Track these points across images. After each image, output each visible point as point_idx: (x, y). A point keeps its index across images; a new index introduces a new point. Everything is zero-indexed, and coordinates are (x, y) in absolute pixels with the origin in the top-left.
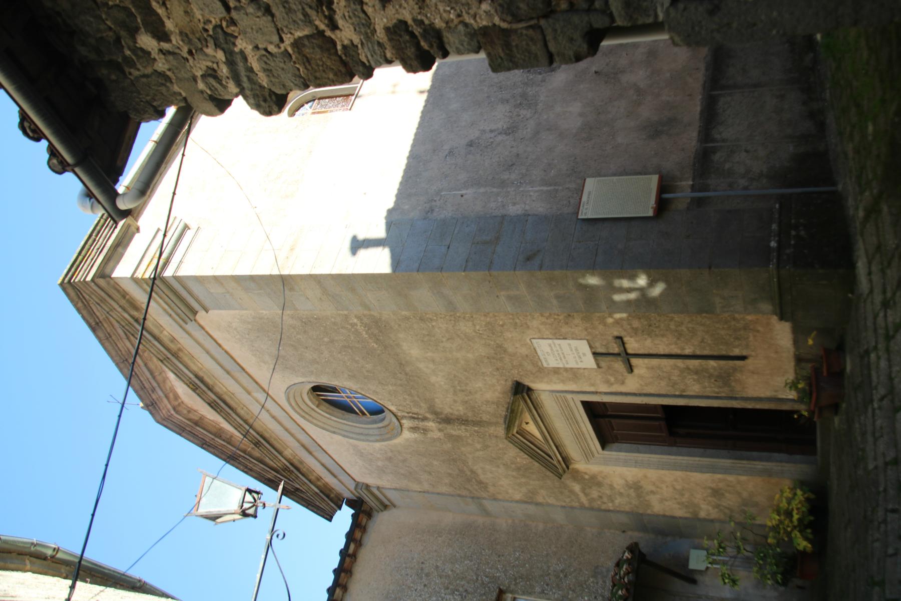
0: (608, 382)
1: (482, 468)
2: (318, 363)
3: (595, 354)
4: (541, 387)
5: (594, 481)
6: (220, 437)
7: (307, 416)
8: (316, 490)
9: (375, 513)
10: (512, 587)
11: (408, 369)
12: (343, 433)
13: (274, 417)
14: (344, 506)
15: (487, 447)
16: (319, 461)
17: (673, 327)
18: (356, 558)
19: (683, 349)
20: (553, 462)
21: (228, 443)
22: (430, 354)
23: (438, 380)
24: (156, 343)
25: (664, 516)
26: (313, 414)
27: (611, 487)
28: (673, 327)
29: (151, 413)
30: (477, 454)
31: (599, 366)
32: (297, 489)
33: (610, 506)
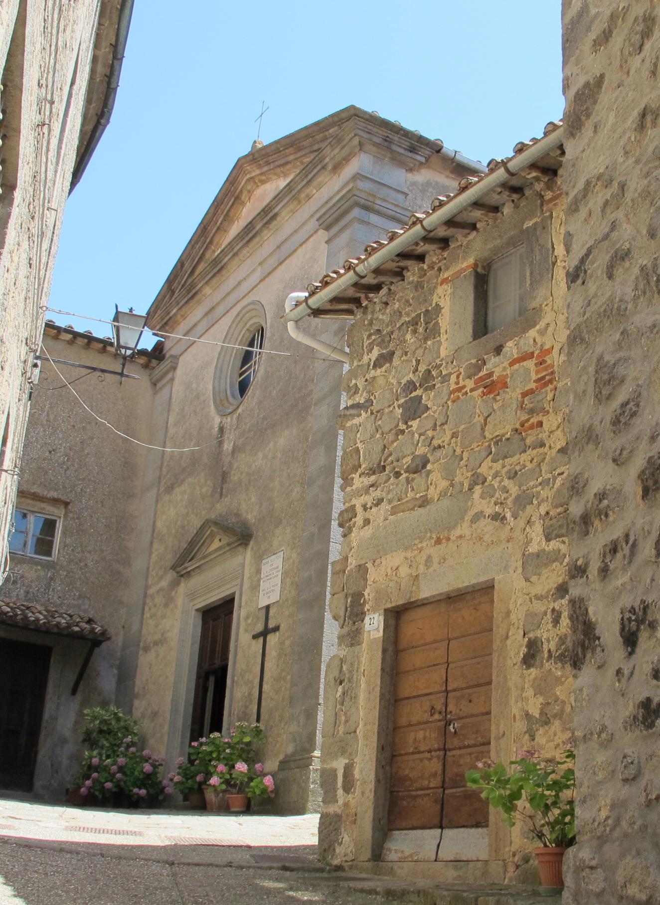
0: (247, 617)
1: (185, 491)
2: (280, 343)
3: (268, 608)
4: (247, 556)
5: (169, 601)
6: (224, 220)
7: (239, 319)
8: (173, 313)
9: (148, 372)
10: (71, 515)
11: (269, 431)
12: (219, 366)
13: (239, 284)
14: (156, 339)
15: (203, 499)
16: (199, 322)
17: (284, 674)
18: (102, 353)
19: (267, 684)
20: (187, 559)
21: (218, 229)
22: (279, 456)
23: (259, 460)
24: (304, 182)
25: (137, 667)
26: (241, 325)
27: (164, 616)
28: (284, 674)
29: (246, 156)
30: (198, 488)
31: (260, 609)
32: (173, 293)
33: (147, 615)
